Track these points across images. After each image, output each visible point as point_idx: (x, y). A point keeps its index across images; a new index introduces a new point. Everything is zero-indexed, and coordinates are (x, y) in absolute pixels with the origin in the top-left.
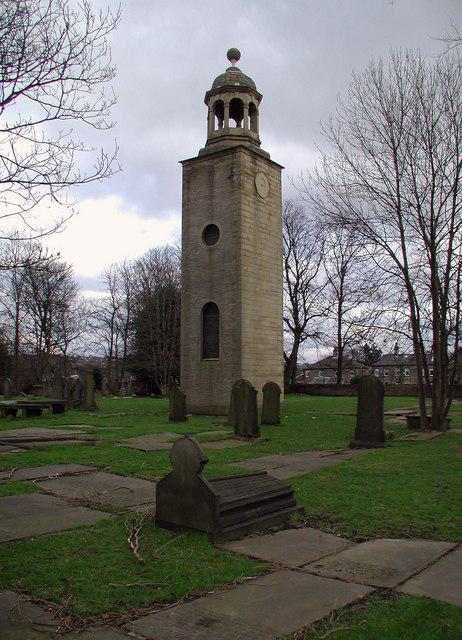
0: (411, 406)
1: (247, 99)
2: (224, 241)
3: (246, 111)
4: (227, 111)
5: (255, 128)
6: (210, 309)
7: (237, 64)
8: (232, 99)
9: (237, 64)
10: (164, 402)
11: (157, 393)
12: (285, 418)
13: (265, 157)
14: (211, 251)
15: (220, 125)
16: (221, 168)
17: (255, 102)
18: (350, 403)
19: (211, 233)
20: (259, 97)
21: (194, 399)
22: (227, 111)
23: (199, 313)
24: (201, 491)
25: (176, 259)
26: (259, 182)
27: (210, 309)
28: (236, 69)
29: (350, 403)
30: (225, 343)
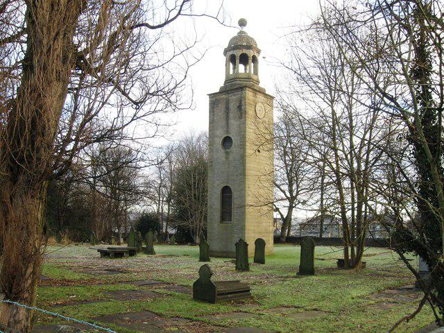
0: (338, 253)
1: (251, 53)
2: (234, 149)
3: (250, 61)
4: (238, 61)
5: (256, 72)
6: (226, 191)
7: (245, 29)
8: (241, 52)
9: (245, 29)
10: (197, 249)
11: (193, 243)
12: (267, 260)
13: (262, 92)
14: (227, 153)
15: (234, 68)
16: (233, 98)
17: (256, 54)
18: (297, 249)
19: (227, 141)
20: (259, 52)
21: (215, 245)
22: (238, 61)
23: (220, 193)
24: (211, 286)
25: (205, 147)
26: (258, 108)
27: (226, 191)
28: (244, 33)
29: (297, 249)
30: (234, 211)
